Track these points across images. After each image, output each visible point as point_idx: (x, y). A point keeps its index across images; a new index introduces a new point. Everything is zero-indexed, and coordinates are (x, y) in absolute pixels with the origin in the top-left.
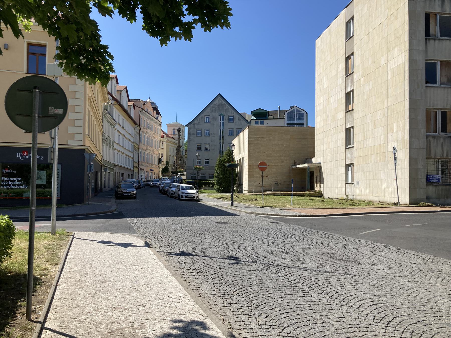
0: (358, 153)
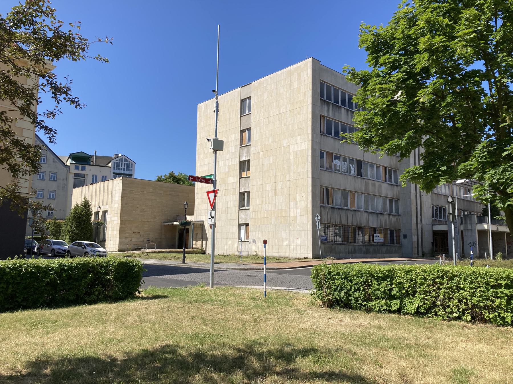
0: (255, 215)
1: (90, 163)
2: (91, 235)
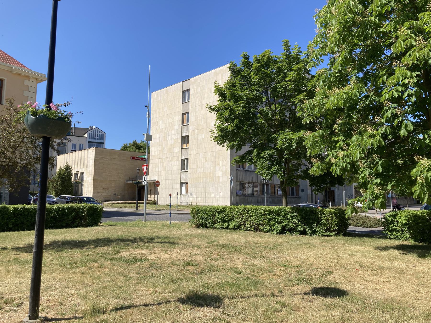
1: (70, 134)
2: (72, 191)
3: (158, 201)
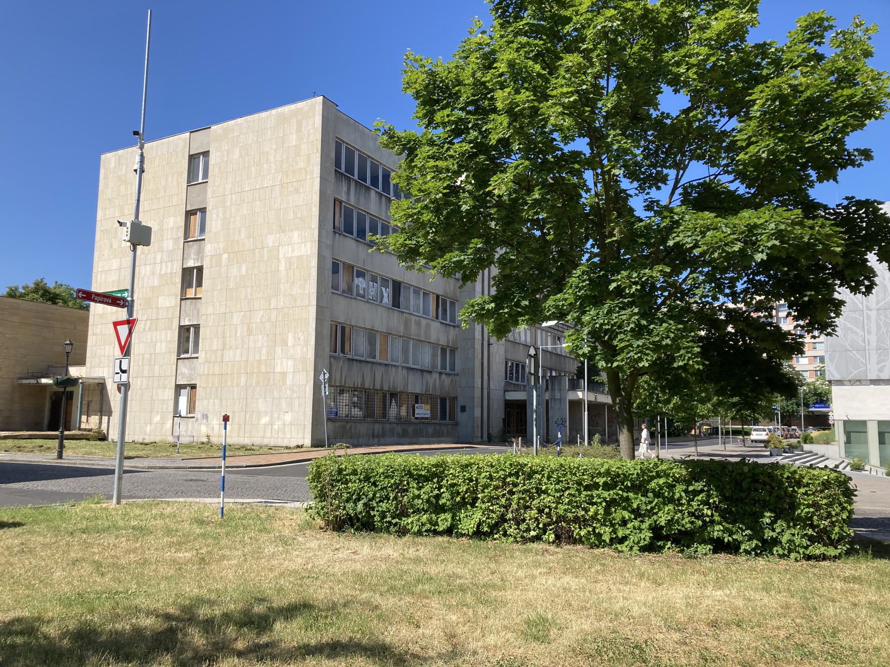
3: (111, 432)
